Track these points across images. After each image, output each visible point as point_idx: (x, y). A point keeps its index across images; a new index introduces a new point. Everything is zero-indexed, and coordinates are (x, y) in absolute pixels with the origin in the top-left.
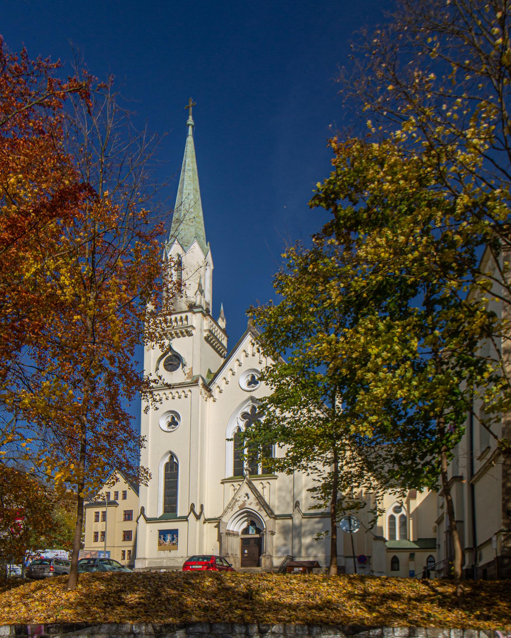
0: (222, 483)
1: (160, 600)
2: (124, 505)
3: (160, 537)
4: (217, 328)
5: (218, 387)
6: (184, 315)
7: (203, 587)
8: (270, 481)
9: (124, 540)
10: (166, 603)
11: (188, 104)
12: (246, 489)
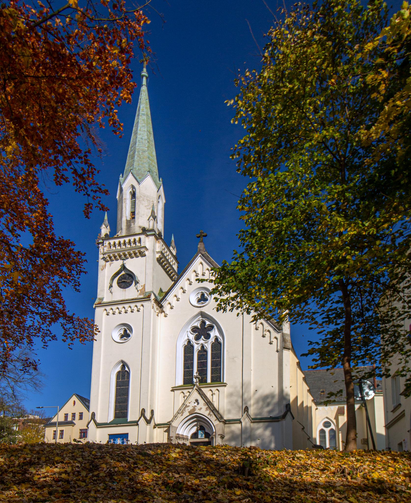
0: (173, 390)
1: (97, 476)
4: (168, 253)
5: (170, 304)
6: (137, 238)
7: (168, 460)
10: (108, 479)
12: (195, 395)
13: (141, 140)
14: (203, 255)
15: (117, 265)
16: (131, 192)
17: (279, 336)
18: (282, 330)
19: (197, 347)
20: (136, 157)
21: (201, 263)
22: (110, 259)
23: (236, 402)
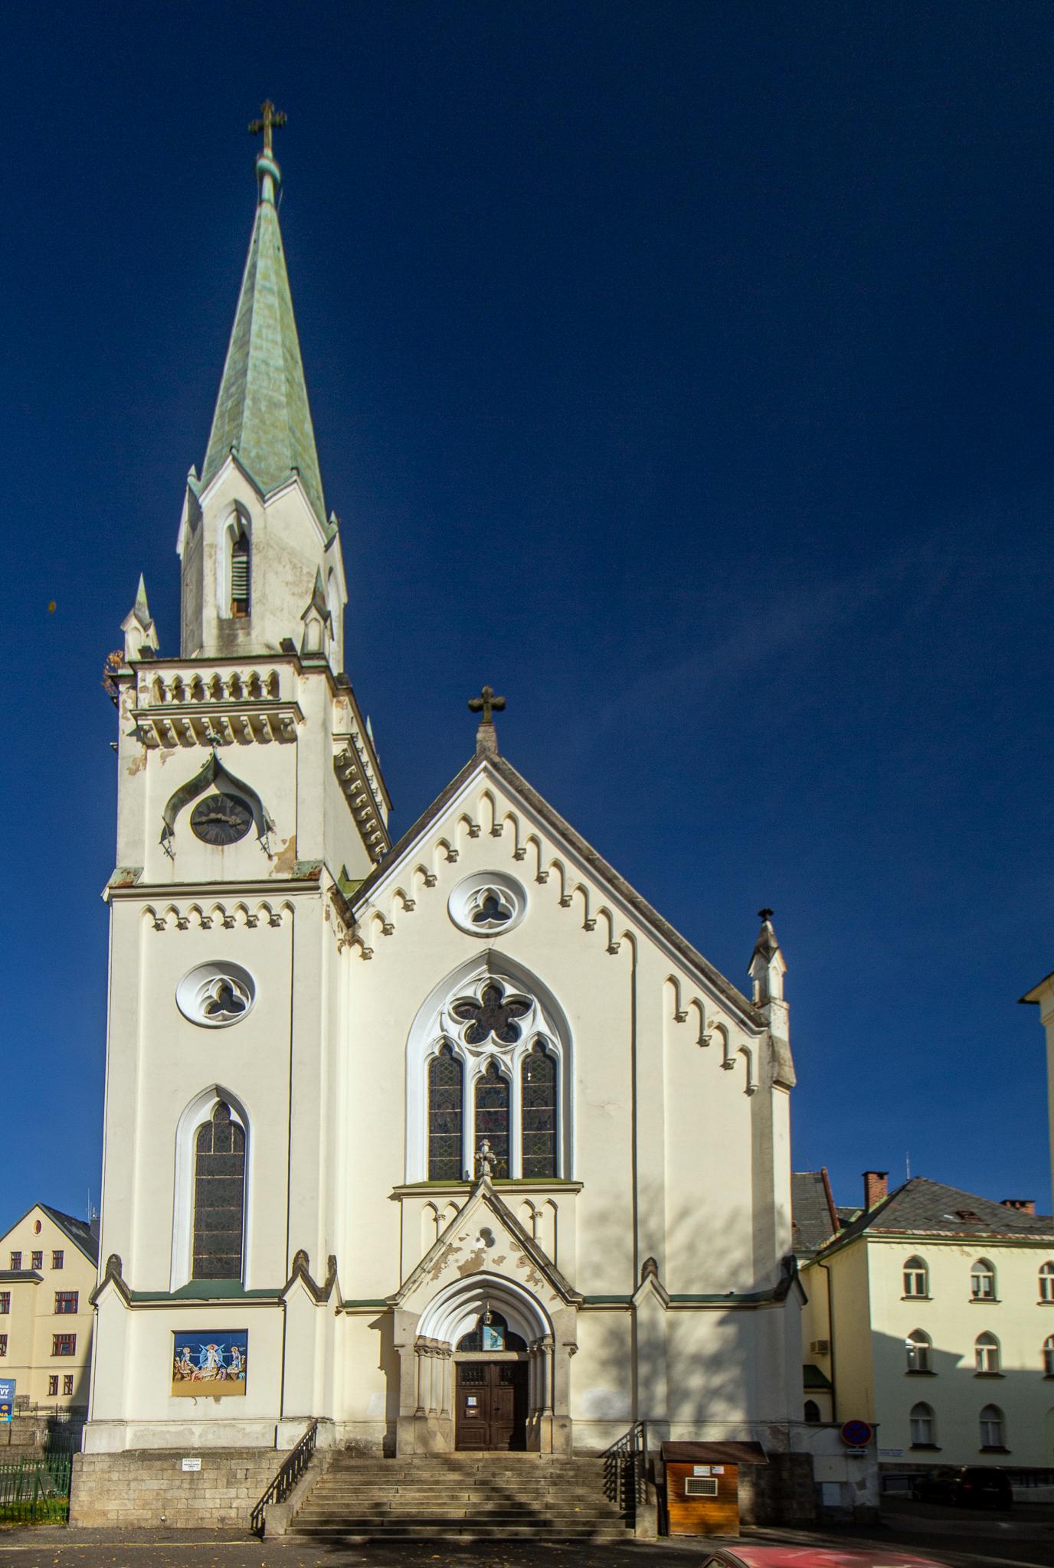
0: (396, 1197)
2: (54, 1281)
3: (178, 1354)
5: (379, 916)
8: (556, 1198)
9: (56, 1353)
11: (261, 116)
12: (480, 1214)
13: (263, 368)
14: (495, 765)
15: (190, 761)
16: (231, 527)
17: (754, 1044)
18: (768, 1025)
19: (474, 1067)
20: (247, 413)
21: (488, 794)
22: (161, 737)
23: (619, 1243)
